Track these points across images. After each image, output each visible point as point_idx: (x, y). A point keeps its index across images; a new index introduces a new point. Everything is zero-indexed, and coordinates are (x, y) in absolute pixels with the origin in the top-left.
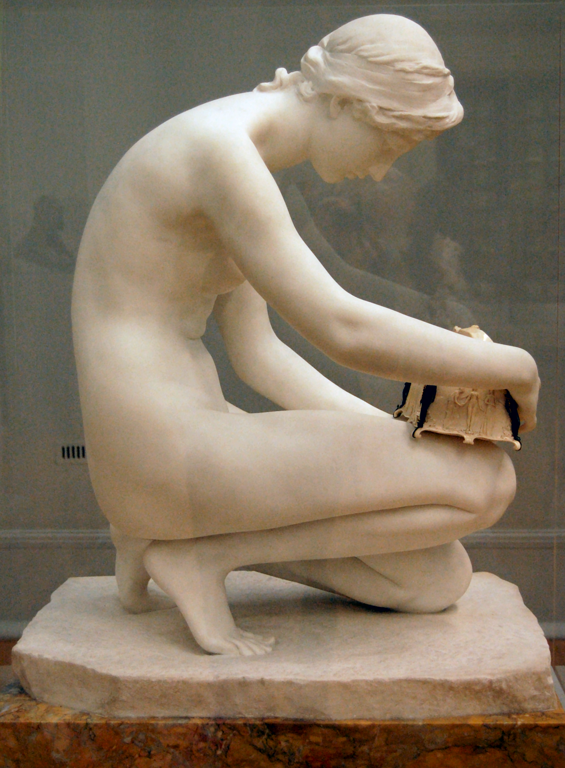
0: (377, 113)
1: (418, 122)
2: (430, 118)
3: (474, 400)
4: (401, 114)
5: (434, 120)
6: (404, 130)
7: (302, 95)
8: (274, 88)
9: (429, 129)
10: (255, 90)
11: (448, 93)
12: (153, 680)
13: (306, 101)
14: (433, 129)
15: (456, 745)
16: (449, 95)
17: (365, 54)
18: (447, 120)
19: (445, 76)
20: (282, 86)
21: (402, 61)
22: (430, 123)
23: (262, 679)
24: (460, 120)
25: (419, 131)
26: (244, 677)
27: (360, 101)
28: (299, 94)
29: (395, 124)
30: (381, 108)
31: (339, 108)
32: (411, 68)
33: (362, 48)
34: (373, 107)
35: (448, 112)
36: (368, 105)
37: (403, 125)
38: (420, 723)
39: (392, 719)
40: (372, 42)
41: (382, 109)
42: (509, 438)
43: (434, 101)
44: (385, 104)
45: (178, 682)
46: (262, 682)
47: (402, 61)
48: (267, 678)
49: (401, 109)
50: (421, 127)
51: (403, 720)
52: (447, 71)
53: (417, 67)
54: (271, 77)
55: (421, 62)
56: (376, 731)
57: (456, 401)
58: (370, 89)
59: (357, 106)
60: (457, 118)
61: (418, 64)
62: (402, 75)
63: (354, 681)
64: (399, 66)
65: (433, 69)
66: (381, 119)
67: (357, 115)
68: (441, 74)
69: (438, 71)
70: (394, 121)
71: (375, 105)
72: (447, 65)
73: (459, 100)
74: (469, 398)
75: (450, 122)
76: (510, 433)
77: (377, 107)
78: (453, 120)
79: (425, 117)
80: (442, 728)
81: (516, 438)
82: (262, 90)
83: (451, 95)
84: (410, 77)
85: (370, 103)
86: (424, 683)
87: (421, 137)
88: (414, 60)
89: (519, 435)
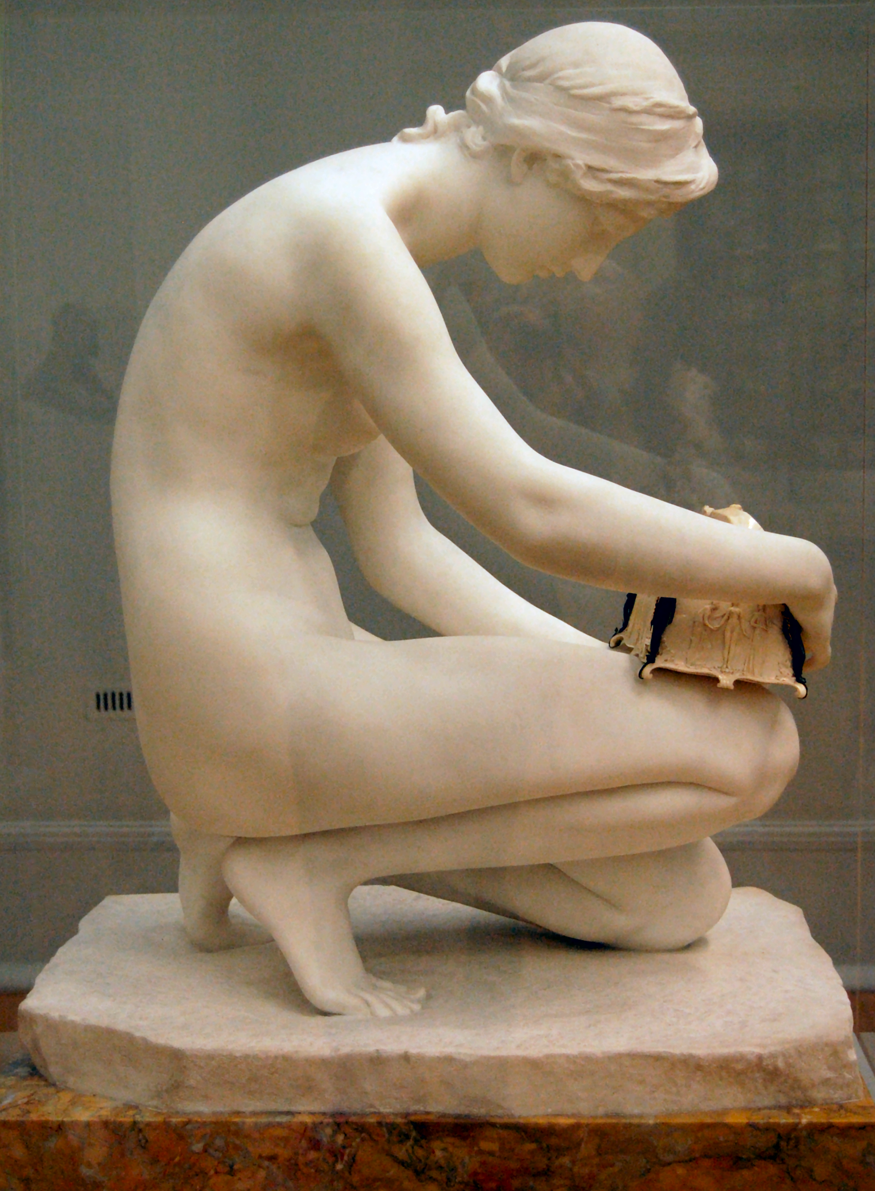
0: (585, 175)
1: (647, 190)
2: (666, 184)
3: (734, 620)
4: (621, 177)
5: (672, 187)
6: (625, 202)
7: (467, 148)
8: (425, 137)
9: (664, 200)
10: (395, 139)
11: (694, 144)
12: (238, 1055)
13: (475, 156)
14: (671, 200)
15: (706, 1156)
16: (696, 147)
17: (565, 83)
18: (693, 187)
19: (690, 117)
20: (436, 133)
21: (623, 94)
22: (666, 191)
23: (406, 1053)
24: (713, 187)
25: (650, 204)
26: (377, 1051)
27: (558, 156)
28: (464, 146)
29: (611, 192)
30: (590, 168)
31: (525, 167)
32: (636, 106)
33: (560, 74)
34: (577, 166)
35: (693, 173)
36: (570, 162)
37: (624, 193)
38: (651, 1122)
39: (607, 1116)
40: (576, 65)
41: (591, 170)
42: (788, 679)
43: (673, 156)
44: (597, 160)
45: (276, 1057)
46: (406, 1057)
47: (623, 94)
48: (413, 1051)
49: (621, 170)
50: (652, 197)
51: (624, 1117)
52: (692, 109)
53: (646, 104)
54: (419, 120)
55: (652, 95)
56: (582, 1133)
57: (707, 622)
58: (574, 138)
59: (553, 164)
60: (707, 183)
61: (647, 99)
62: (623, 116)
63: (548, 1057)
64: (618, 102)
65: (671, 107)
66: (590, 185)
67: (553, 178)
68: (683, 115)
69: (678, 109)
70: (609, 187)
71: (580, 162)
72: (692, 100)
73: (710, 156)
74: (726, 617)
75: (698, 189)
76: (789, 671)
77: (583, 166)
78: (701, 186)
79: (658, 182)
80: (684, 1129)
81: (799, 679)
82: (406, 140)
83: (699, 148)
84: (635, 119)
85: (573, 159)
86: (657, 1058)
87: (652, 212)
88: (642, 94)
89: (804, 674)
